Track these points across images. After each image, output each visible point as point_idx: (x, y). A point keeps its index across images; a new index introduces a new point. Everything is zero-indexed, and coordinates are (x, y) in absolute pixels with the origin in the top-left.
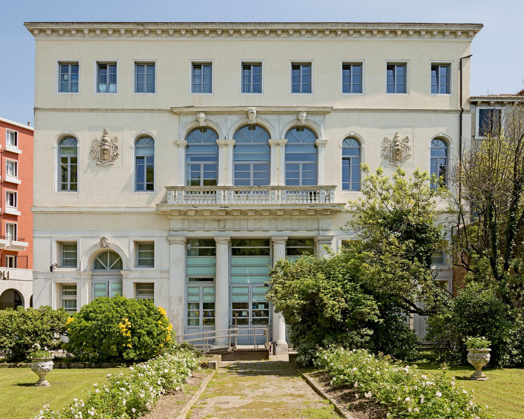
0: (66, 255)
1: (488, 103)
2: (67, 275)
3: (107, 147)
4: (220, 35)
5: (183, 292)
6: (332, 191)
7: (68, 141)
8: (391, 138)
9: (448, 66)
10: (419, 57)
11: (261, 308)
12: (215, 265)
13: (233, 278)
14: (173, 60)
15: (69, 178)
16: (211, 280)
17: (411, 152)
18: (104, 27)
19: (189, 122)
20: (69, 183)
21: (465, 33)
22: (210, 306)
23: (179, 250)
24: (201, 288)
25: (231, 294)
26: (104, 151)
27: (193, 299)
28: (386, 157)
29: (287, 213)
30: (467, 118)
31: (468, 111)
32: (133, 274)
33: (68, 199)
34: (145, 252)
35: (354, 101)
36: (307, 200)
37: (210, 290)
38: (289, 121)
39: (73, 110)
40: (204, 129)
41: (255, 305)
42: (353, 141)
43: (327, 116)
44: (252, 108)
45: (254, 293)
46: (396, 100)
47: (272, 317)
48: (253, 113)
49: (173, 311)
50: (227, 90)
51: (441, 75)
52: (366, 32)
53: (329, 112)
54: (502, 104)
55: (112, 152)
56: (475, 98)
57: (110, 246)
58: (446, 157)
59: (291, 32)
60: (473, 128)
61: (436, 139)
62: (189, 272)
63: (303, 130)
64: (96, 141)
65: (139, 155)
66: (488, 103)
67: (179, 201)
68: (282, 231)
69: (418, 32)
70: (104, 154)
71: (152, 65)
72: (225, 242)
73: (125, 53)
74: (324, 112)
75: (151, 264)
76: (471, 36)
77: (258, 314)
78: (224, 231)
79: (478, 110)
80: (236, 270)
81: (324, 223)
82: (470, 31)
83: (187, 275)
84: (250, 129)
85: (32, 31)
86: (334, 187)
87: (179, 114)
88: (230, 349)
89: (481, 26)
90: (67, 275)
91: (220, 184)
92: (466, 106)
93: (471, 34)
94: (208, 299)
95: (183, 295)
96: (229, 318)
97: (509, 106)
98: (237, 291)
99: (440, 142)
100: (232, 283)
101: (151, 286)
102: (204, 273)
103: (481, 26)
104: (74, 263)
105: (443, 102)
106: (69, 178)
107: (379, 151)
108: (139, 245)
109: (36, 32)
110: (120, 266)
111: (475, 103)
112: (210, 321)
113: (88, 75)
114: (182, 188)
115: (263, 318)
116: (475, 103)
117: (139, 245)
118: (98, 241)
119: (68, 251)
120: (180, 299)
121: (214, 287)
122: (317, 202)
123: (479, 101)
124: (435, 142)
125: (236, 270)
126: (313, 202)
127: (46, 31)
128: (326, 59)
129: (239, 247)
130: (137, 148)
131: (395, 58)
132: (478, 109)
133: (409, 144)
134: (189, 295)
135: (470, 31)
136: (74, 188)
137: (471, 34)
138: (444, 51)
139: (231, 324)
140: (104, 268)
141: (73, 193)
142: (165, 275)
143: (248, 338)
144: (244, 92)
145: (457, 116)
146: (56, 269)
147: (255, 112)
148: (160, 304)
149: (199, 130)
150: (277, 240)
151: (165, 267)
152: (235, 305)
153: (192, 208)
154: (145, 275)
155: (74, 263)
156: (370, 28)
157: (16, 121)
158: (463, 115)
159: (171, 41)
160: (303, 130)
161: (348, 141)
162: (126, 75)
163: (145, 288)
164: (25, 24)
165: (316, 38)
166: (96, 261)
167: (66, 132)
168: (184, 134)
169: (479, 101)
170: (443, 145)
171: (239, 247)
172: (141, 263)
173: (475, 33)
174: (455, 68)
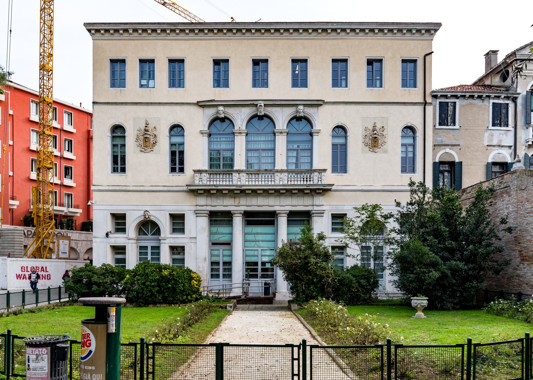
0: (117, 224)
1: (446, 97)
2: (119, 239)
3: (148, 136)
4: (234, 34)
5: (207, 254)
6: (323, 174)
7: (118, 131)
8: (371, 128)
9: (415, 61)
10: (393, 52)
11: (268, 266)
12: (232, 234)
13: (246, 242)
14: (198, 57)
15: (119, 163)
16: (214, 244)
17: (385, 140)
18: (144, 27)
19: (210, 113)
20: (177, 166)
21: (428, 31)
22: (228, 264)
23: (204, 221)
24: (221, 251)
25: (245, 256)
26: (146, 140)
27: (215, 259)
28: (366, 145)
29: (289, 192)
30: (429, 109)
31: (431, 104)
32: (168, 238)
33: (118, 179)
34: (178, 221)
35: (340, 94)
36: (300, 181)
37: (227, 253)
38: (289, 112)
39: (122, 103)
40: (223, 120)
41: (263, 264)
42: (341, 130)
43: (319, 108)
44: (260, 102)
45: (265, 255)
46: (374, 94)
47: (276, 273)
48: (261, 106)
49: (199, 268)
50: (241, 85)
51: (413, 70)
52: (351, 30)
53: (321, 105)
54: (456, 97)
55: (152, 140)
56: (435, 92)
57: (151, 217)
58: (177, 145)
59: (376, 31)
60: (434, 118)
61: (405, 128)
62: (211, 239)
63: (301, 121)
64: (139, 130)
65: (115, 143)
66: (446, 97)
67: (205, 181)
68: (284, 206)
69: (391, 31)
70: (147, 141)
71: (182, 61)
72: (205, 215)
73: (161, 50)
74: (317, 104)
75: (182, 231)
76: (432, 34)
77: (266, 270)
78: (239, 206)
79: (438, 103)
80: (249, 237)
81: (319, 200)
82: (431, 29)
83: (210, 240)
84: (259, 119)
85: (89, 31)
86: (325, 170)
87: (203, 106)
88: (243, 297)
89: (439, 25)
90: (119, 239)
91: (236, 168)
92: (429, 99)
93: (433, 32)
94: (227, 259)
95: (207, 256)
96: (243, 273)
97: (461, 98)
98: (248, 253)
99: (409, 131)
100: (245, 247)
101: (183, 248)
102: (225, 239)
103: (439, 25)
104: (123, 230)
105: (415, 94)
106: (119, 163)
107: (360, 139)
108: (173, 217)
109: (93, 32)
110: (158, 232)
111: (435, 97)
112: (228, 275)
113: (132, 72)
114: (206, 171)
115: (268, 272)
116: (435, 97)
117: (173, 217)
118: (142, 213)
119: (119, 221)
120: (205, 259)
121: (231, 250)
122: (312, 183)
123: (439, 94)
124: (405, 130)
125: (249, 237)
126: (308, 183)
127: (166, 31)
128: (320, 55)
129: (252, 218)
130: (171, 136)
131: (375, 55)
132: (438, 101)
133: (384, 133)
134: (212, 255)
135: (431, 29)
136: (123, 170)
137: (433, 32)
138: (412, 48)
139: (245, 278)
140: (147, 235)
141: (181, 174)
142: (193, 240)
143: (256, 287)
144: (219, 86)
145: (422, 107)
146: (110, 235)
147: (263, 105)
148: (189, 264)
149: (219, 120)
150: (280, 213)
151: (193, 235)
152: (248, 264)
153: (214, 188)
154: (178, 240)
155: (123, 230)
156: (353, 27)
157: (459, 114)
158: (426, 107)
159: (205, 39)
160: (301, 121)
161: (336, 130)
162: (162, 71)
163: (177, 250)
164: (86, 25)
165: (160, 37)
166: (140, 229)
167: (117, 123)
168: (207, 124)
169: (439, 94)
170: (411, 133)
171: (252, 218)
172: (174, 231)
173: (436, 31)
174: (420, 64)
